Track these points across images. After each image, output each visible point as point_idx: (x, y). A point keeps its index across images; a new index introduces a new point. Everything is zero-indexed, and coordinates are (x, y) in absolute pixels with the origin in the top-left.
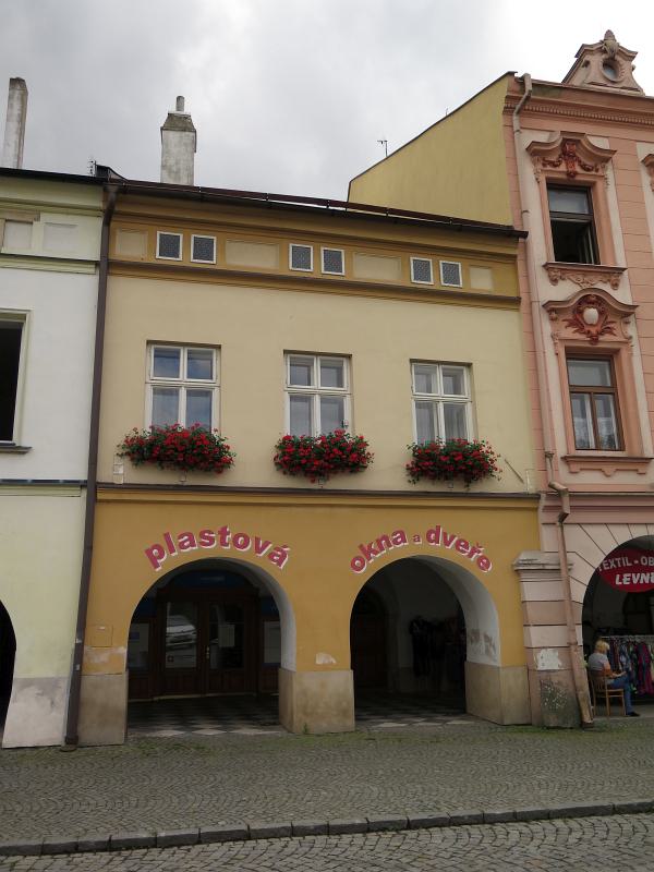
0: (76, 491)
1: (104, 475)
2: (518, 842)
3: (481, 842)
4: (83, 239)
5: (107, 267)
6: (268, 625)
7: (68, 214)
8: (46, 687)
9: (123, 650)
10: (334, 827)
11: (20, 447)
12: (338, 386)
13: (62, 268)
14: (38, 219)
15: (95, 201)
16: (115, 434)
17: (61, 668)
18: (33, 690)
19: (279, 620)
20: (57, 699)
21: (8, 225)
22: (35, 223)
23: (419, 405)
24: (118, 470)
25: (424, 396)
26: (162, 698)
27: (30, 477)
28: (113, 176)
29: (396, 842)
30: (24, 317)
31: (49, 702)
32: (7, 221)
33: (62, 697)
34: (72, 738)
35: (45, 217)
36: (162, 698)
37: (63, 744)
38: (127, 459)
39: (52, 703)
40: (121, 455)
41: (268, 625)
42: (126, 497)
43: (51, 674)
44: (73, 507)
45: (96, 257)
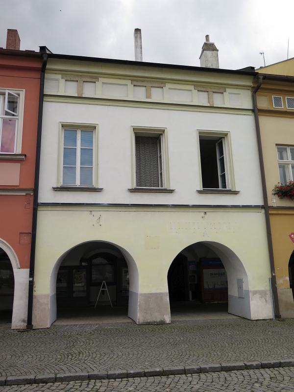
0: (259, 210)
1: (270, 204)
2: (243, 381)
3: (243, 381)
4: (244, 100)
5: (256, 112)
6: (124, 269)
7: (237, 88)
8: (262, 294)
9: (288, 278)
10: (189, 370)
11: (235, 191)
12: (281, 159)
13: (74, 101)
14: (225, 91)
15: (248, 82)
16: (271, 187)
17: (266, 286)
18: (258, 296)
19: (127, 268)
20: (267, 299)
21: (85, 83)
22: (97, 82)
23: (280, 167)
24: (274, 201)
25: (282, 161)
26: (219, 302)
27: (241, 204)
28: (48, 52)
29: (62, 386)
30: (164, 131)
31: (264, 300)
32: (84, 82)
33: (269, 297)
34: (277, 315)
35: (101, 80)
36: (219, 302)
37: (26, 328)
38: (276, 196)
39: (266, 301)
40: (274, 194)
41: (124, 269)
42: (280, 212)
43: (263, 289)
44: (258, 218)
45: (251, 107)
